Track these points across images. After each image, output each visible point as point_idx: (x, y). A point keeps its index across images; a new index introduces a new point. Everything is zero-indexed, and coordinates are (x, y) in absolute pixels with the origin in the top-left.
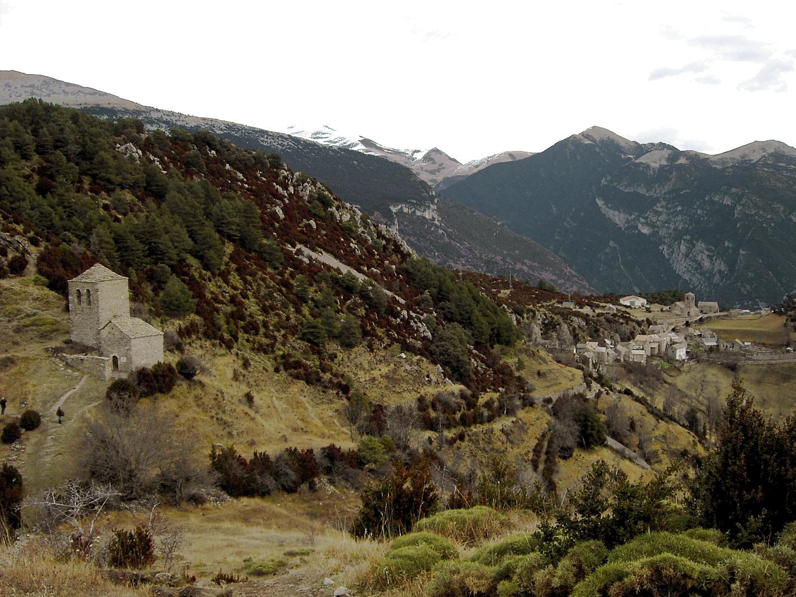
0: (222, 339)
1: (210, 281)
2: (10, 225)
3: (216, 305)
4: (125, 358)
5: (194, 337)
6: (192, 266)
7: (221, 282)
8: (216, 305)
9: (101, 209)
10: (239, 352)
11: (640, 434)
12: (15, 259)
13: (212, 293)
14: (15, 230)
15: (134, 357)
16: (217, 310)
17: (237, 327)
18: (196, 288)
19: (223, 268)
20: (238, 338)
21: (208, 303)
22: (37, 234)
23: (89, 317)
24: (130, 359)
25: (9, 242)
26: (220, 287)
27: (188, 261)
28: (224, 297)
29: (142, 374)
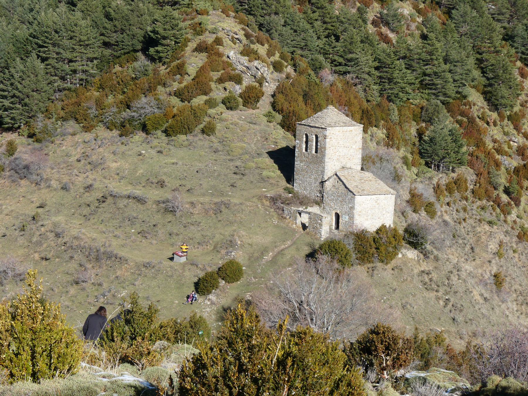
0: (497, 202)
1: (495, 124)
2: (252, 46)
3: (498, 157)
4: (347, 217)
5: (457, 195)
6: (474, 105)
7: (510, 128)
8: (498, 157)
9: (371, 26)
10: (518, 220)
11: (55, 190)
12: (249, 88)
13: (495, 141)
14: (256, 53)
15: (356, 217)
16: (498, 165)
17: (522, 188)
18: (471, 129)
19: (517, 109)
20: (520, 201)
21: (488, 154)
22: (282, 57)
23: (75, 66)
24: (352, 218)
25: (247, 68)
26: (506, 134)
27: (470, 99)
28: (510, 147)
29: (360, 237)
